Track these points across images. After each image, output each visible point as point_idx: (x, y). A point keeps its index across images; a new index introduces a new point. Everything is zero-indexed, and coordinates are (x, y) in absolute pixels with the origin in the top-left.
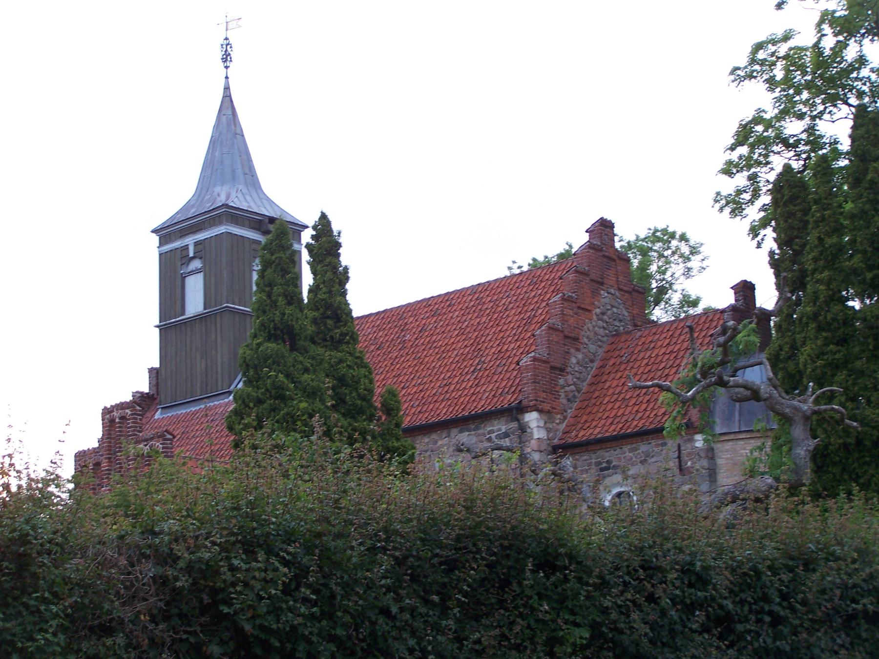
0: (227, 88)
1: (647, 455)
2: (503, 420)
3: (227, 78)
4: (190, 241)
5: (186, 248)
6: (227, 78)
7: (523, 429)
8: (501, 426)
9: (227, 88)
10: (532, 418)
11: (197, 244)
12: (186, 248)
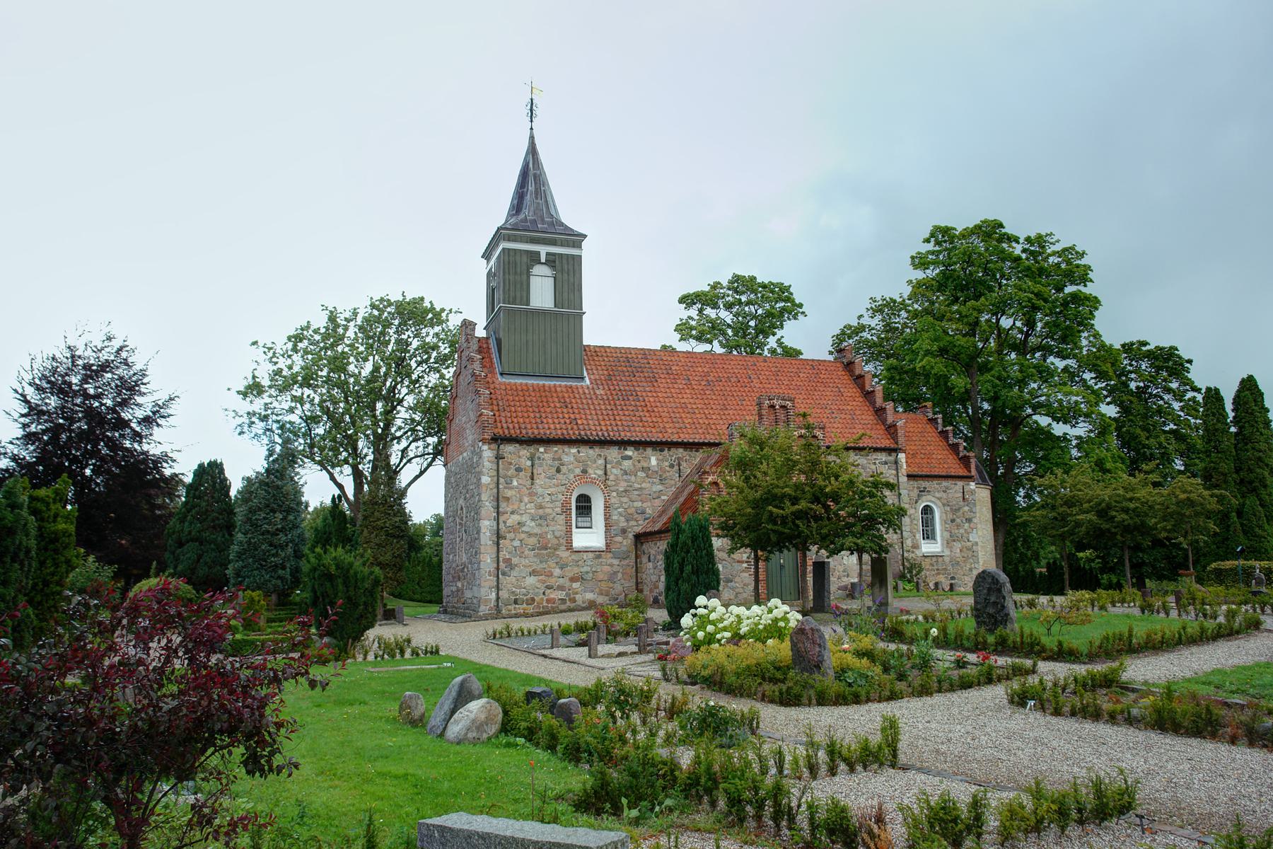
0: (532, 138)
1: (947, 488)
2: (884, 454)
3: (532, 129)
4: (543, 250)
5: (538, 253)
6: (532, 129)
7: (896, 462)
8: (883, 457)
9: (532, 138)
10: (902, 456)
11: (548, 254)
12: (538, 253)
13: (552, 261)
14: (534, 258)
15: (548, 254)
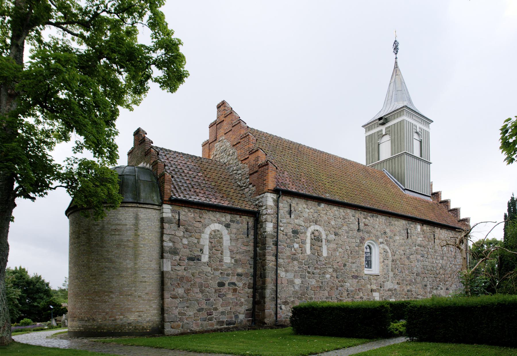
0: (396, 63)
6: (396, 58)
9: (396, 63)
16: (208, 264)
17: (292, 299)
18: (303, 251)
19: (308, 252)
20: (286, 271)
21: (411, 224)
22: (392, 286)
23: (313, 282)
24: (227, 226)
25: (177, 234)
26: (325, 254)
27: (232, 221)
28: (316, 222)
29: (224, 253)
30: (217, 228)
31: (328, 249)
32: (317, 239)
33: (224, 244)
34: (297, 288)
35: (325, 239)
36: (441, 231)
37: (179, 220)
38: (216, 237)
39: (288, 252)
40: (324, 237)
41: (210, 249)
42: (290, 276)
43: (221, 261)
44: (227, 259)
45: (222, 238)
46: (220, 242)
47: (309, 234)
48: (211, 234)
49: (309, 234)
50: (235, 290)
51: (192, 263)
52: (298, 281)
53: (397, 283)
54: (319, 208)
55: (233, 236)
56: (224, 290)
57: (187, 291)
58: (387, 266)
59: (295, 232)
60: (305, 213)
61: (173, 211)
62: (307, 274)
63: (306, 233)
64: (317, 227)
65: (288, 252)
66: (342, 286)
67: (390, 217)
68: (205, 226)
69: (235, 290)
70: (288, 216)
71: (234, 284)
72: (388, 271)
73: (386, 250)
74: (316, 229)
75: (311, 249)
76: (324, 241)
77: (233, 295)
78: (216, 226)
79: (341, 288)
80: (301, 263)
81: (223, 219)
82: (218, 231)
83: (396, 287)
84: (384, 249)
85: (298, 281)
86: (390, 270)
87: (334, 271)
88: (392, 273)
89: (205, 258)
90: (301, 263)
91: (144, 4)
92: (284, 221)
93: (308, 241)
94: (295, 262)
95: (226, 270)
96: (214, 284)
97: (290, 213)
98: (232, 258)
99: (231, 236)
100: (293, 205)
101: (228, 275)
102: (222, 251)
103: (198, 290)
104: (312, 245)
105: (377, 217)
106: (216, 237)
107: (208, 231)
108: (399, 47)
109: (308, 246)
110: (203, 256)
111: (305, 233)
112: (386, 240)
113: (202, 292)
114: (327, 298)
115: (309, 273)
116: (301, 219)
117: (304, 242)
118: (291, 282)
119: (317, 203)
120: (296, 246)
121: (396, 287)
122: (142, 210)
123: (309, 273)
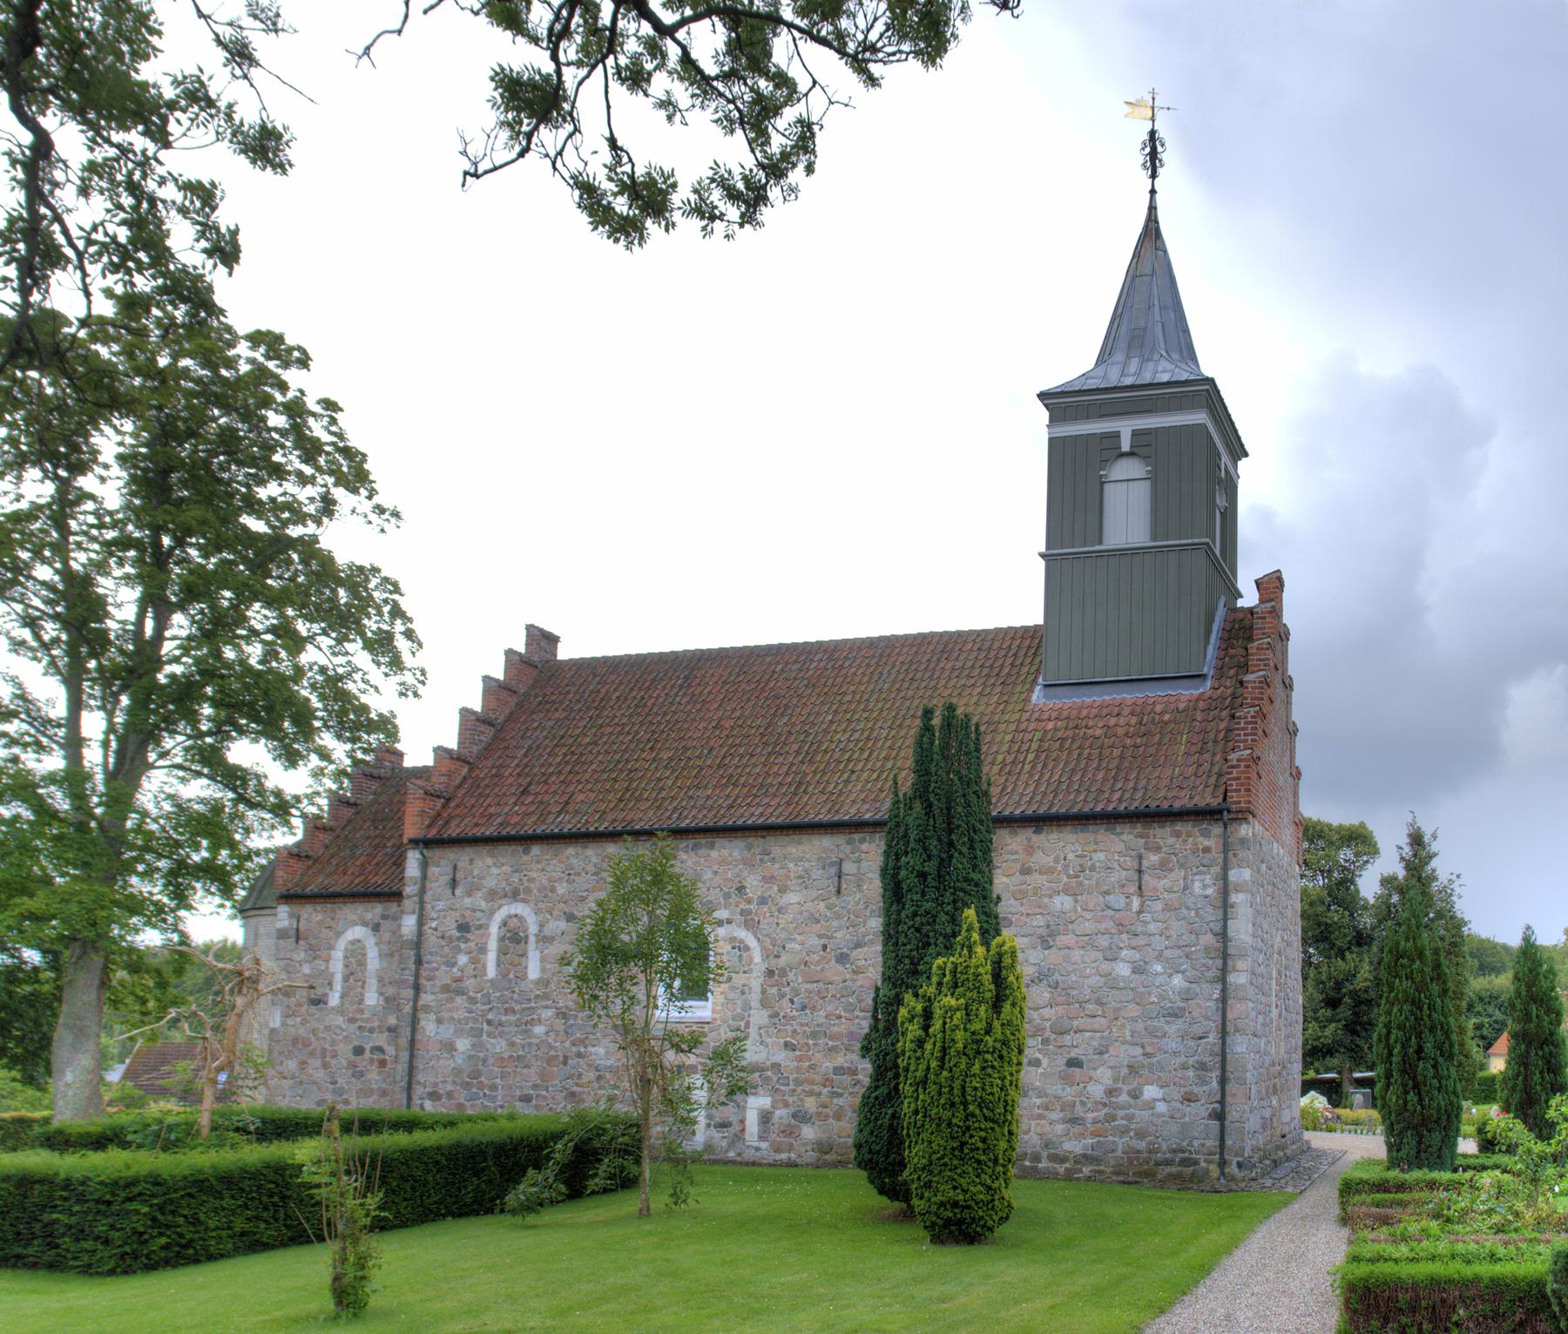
0: (1152, 208)
3: (1153, 192)
4: (1126, 428)
6: (1153, 192)
9: (1152, 208)
13: (1144, 445)
14: (1108, 448)
15: (1135, 434)
16: (340, 1010)
17: (449, 1087)
18: (480, 969)
19: (491, 972)
20: (439, 1021)
21: (862, 841)
22: (764, 1055)
23: (499, 1046)
24: (376, 928)
25: (295, 957)
26: (534, 972)
27: (385, 917)
28: (515, 895)
29: (367, 986)
30: (357, 936)
31: (543, 960)
32: (514, 937)
33: (369, 967)
34: (460, 1061)
35: (536, 936)
36: (1035, 838)
37: (298, 930)
38: (356, 955)
39: (444, 976)
40: (533, 929)
41: (346, 979)
42: (446, 1032)
43: (361, 1001)
44: (372, 998)
45: (365, 955)
46: (362, 963)
47: (494, 930)
48: (346, 949)
49: (494, 930)
50: (383, 1063)
51: (313, 1009)
52: (463, 1044)
53: (786, 1045)
54: (525, 858)
55: (385, 947)
56: (362, 1062)
57: (303, 1065)
58: (743, 993)
59: (464, 928)
60: (488, 878)
61: (291, 916)
62: (485, 1027)
63: (488, 925)
64: (518, 908)
65: (444, 976)
66: (579, 1055)
67: (763, 837)
68: (339, 934)
69: (383, 1063)
70: (450, 892)
71: (380, 1049)
72: (747, 1007)
73: (742, 941)
74: (513, 912)
75: (498, 965)
76: (532, 939)
77: (380, 1073)
78: (357, 932)
79: (577, 1060)
80: (472, 1001)
81: (369, 916)
82: (359, 941)
83: (781, 1057)
84: (733, 939)
85: (463, 1044)
86: (755, 1004)
87: (558, 1014)
88: (765, 1013)
89: (334, 1000)
90: (472, 1001)
91: (100, 664)
92: (441, 905)
93: (493, 945)
94: (460, 1001)
95: (368, 1020)
96: (345, 1050)
97: (454, 883)
98: (381, 994)
99: (380, 949)
100: (460, 865)
101: (371, 1030)
102: (364, 982)
103: (317, 1063)
104: (502, 952)
105: (712, 846)
106: (356, 955)
107: (342, 944)
108: (1139, 157)
109: (491, 958)
110: (331, 994)
111: (487, 926)
112: (743, 912)
113: (325, 1066)
114: (535, 1087)
115: (489, 1022)
116: (479, 894)
117: (483, 950)
118: (450, 1047)
119: (520, 849)
120: (463, 959)
121: (781, 1057)
122: (261, 919)
123: (489, 1022)
